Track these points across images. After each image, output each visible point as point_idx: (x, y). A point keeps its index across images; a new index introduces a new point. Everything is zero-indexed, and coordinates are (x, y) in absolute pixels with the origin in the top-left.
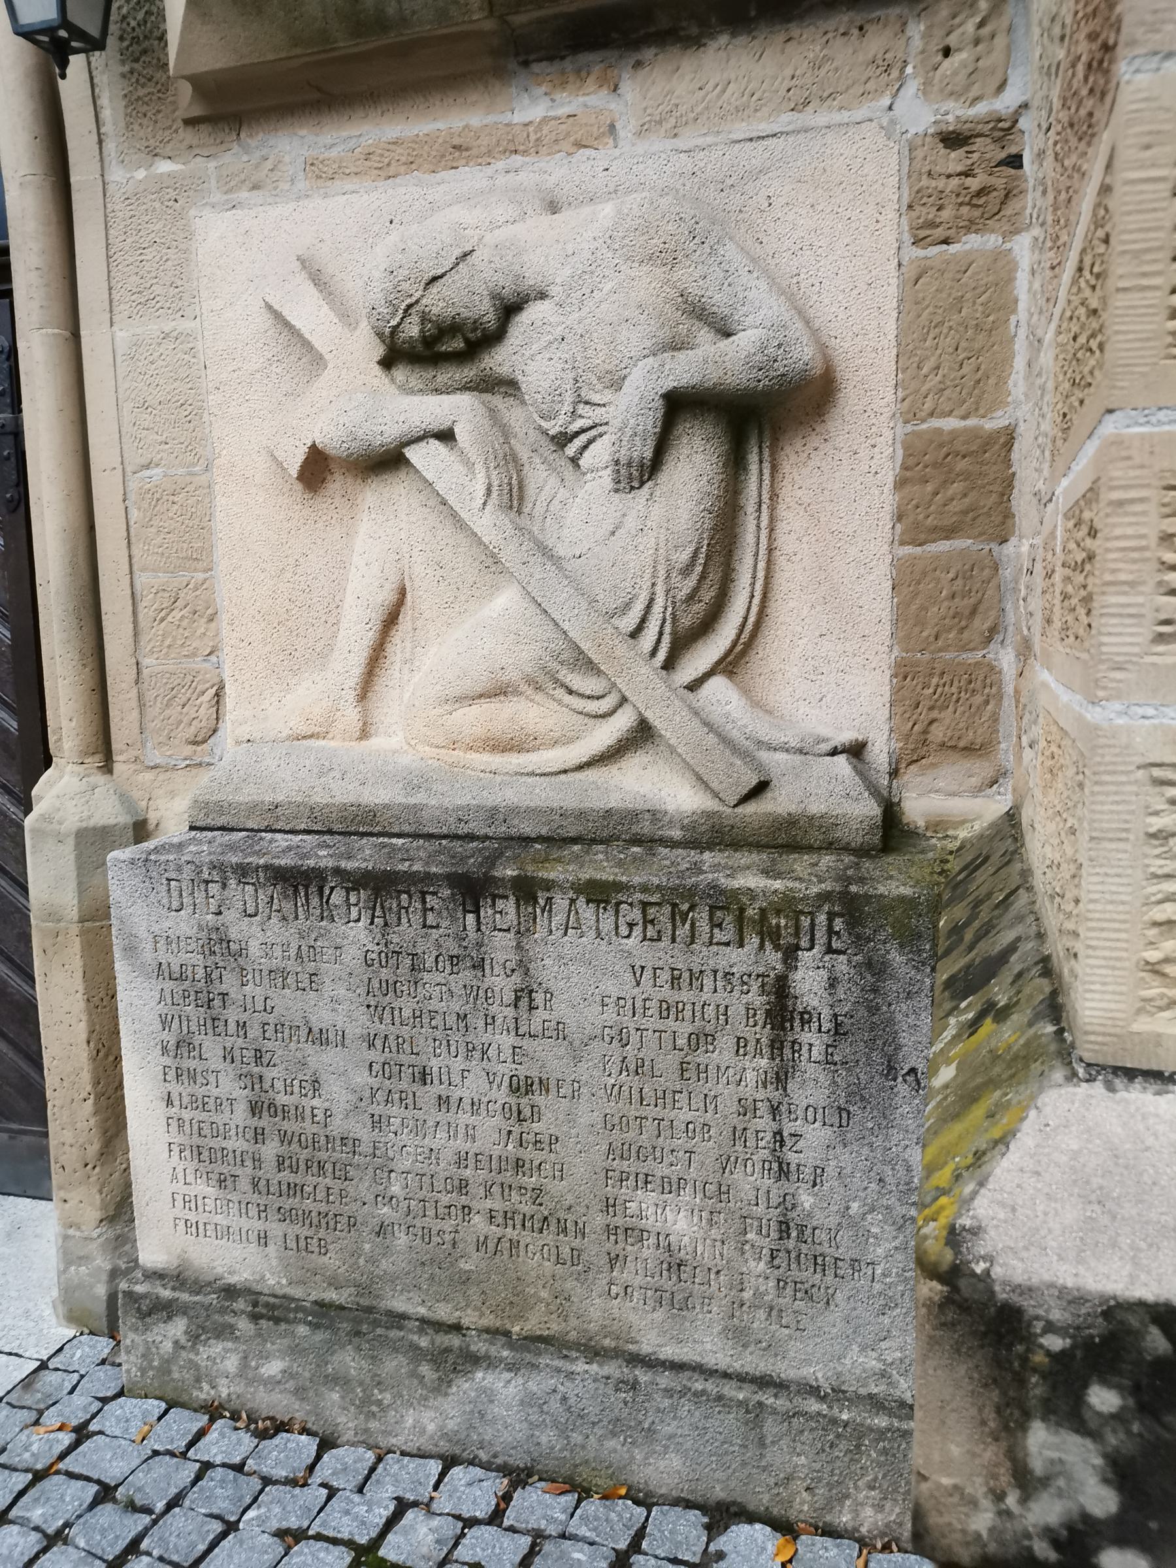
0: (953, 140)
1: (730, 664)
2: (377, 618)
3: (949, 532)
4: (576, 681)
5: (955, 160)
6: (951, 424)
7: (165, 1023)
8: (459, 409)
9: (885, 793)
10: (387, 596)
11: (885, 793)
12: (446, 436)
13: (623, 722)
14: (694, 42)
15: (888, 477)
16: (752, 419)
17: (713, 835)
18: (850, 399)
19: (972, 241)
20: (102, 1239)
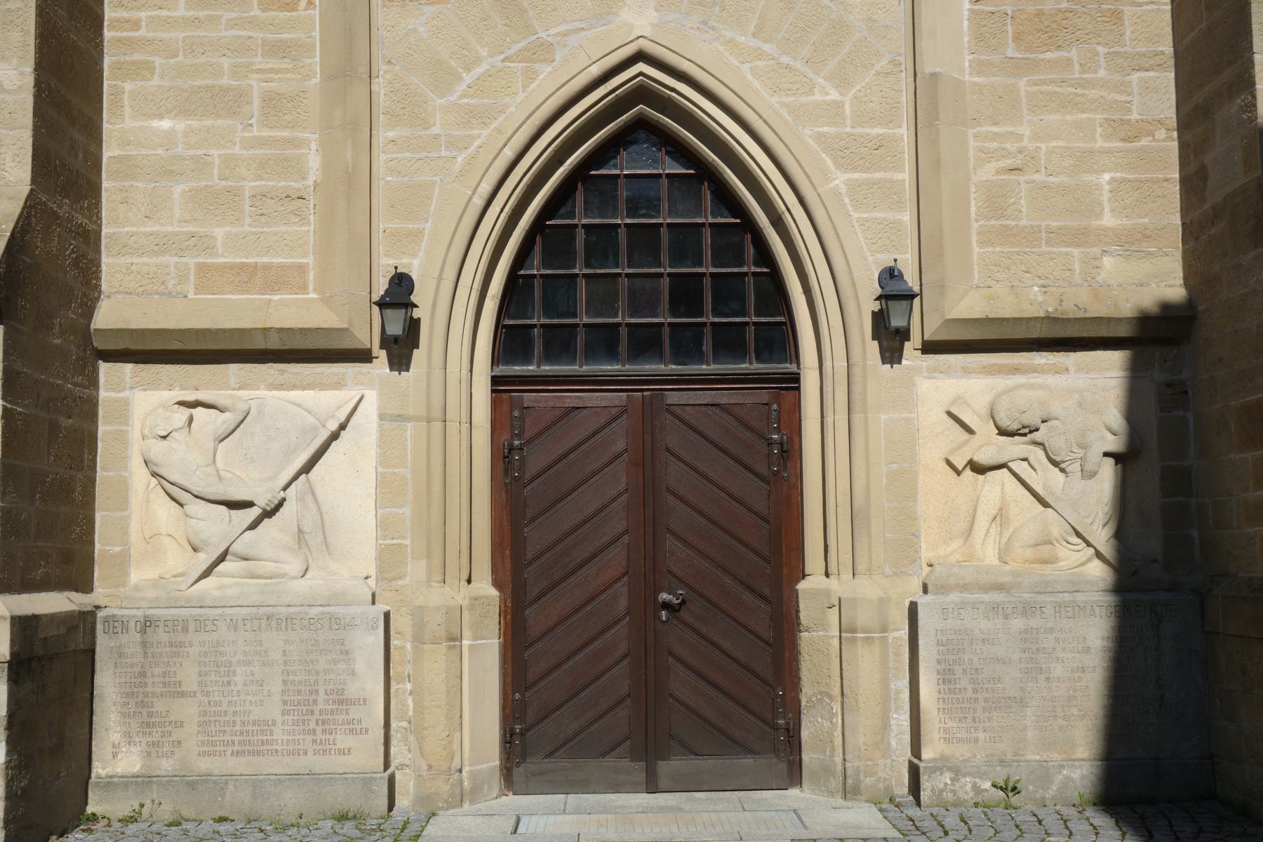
6: (1173, 463)
7: (939, 662)
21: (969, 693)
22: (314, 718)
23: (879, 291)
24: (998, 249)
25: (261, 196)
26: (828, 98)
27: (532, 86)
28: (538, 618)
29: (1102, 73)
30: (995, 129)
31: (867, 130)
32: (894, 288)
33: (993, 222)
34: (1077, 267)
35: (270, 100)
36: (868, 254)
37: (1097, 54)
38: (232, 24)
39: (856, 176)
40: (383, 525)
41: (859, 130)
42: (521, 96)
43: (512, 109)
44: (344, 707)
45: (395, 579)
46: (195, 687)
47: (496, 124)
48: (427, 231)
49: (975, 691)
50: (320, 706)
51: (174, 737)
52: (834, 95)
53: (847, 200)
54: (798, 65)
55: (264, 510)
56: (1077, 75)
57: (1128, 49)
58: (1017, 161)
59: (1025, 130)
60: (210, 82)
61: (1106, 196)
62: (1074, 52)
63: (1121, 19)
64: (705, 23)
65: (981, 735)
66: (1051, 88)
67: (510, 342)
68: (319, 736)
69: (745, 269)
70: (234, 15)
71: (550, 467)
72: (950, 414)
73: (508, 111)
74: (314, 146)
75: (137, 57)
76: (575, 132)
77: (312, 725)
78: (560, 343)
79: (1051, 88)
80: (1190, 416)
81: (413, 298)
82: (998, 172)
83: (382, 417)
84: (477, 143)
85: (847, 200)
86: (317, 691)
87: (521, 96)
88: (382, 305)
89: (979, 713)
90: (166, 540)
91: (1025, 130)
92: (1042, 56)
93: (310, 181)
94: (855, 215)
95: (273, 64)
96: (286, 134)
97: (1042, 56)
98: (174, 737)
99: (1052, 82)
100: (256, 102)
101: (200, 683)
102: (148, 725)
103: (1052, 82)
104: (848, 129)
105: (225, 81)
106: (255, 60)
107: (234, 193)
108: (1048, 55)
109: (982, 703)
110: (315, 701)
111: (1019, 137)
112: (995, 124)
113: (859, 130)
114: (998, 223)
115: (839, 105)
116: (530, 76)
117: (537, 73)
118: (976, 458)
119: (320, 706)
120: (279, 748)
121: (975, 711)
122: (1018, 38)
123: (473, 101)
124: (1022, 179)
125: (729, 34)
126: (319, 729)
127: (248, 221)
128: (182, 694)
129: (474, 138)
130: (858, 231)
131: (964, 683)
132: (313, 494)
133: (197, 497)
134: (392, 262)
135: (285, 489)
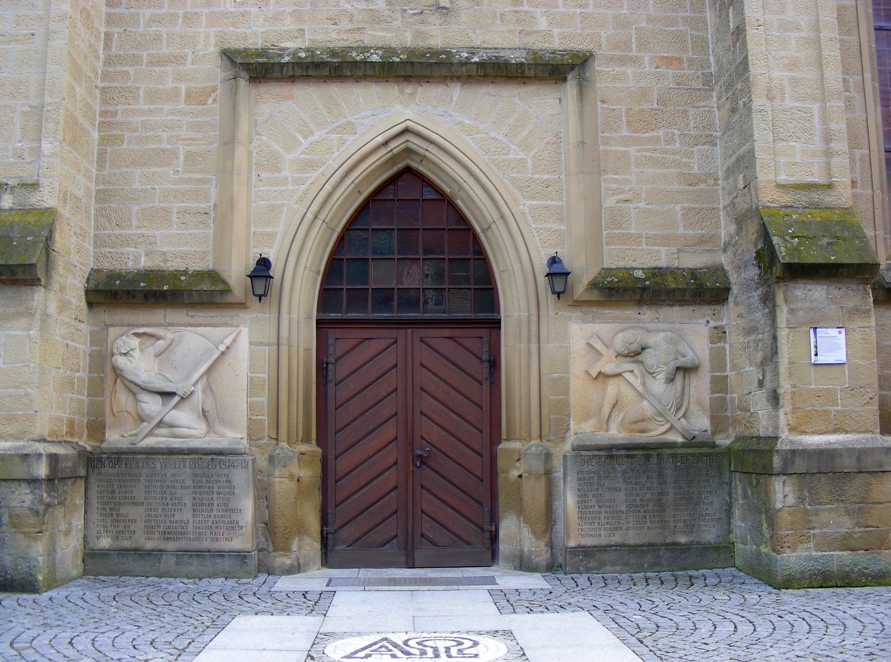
0: (715, 328)
1: (684, 416)
2: (611, 406)
3: (719, 392)
4: (658, 419)
5: (716, 331)
6: (718, 374)
7: (579, 490)
8: (635, 368)
9: (205, 379)
10: (614, 402)
11: (205, 379)
12: (632, 371)
13: (668, 426)
14: (672, 306)
15: (708, 382)
16: (686, 370)
17: (683, 445)
18: (701, 369)
19: (719, 345)
20: (95, 516)
21: (597, 508)
22: (211, 520)
23: (547, 271)
24: (618, 247)
25: (182, 212)
26: (518, 157)
27: (343, 148)
28: (344, 464)
29: (677, 145)
30: (616, 177)
31: (542, 176)
32: (556, 269)
33: (615, 231)
34: (663, 257)
35: (189, 156)
36: (541, 249)
37: (674, 135)
38: (171, 113)
39: (535, 202)
40: (251, 407)
41: (537, 176)
42: (336, 154)
43: (331, 161)
44: (229, 513)
45: (258, 439)
46: (142, 500)
47: (321, 170)
48: (279, 234)
49: (600, 507)
50: (215, 513)
51: (131, 528)
52: (522, 155)
53: (529, 217)
54: (500, 137)
55: (182, 398)
56: (663, 147)
57: (692, 132)
58: (629, 196)
59: (633, 177)
60: (155, 146)
61: (679, 217)
62: (661, 132)
63: (687, 115)
64: (446, 112)
65: (603, 533)
66: (648, 154)
67: (328, 296)
68: (214, 530)
69: (469, 256)
70: (171, 107)
71: (371, 360)
72: (588, 343)
73: (328, 163)
74: (214, 183)
75: (115, 132)
76: (368, 176)
77: (210, 524)
78: (357, 298)
79: (648, 154)
80: (727, 346)
81: (271, 274)
82: (617, 202)
83: (251, 343)
84: (310, 182)
85: (529, 217)
86: (213, 505)
87: (336, 154)
88: (251, 276)
89: (602, 520)
90: (126, 414)
91: (633, 177)
92: (643, 135)
93: (212, 204)
94: (534, 226)
95: (191, 135)
96: (198, 176)
97: (643, 135)
98: (131, 528)
99: (648, 150)
100: (182, 158)
101: (146, 498)
102: (117, 521)
103: (648, 150)
104: (530, 175)
105: (163, 146)
106: (182, 133)
107: (168, 211)
108: (646, 135)
109: (603, 514)
110: (212, 510)
111: (629, 181)
112: (616, 174)
113: (537, 176)
114: (617, 232)
115: (523, 161)
116: (342, 142)
117: (346, 141)
118: (603, 371)
119: (215, 513)
120: (191, 536)
121: (600, 518)
122: (629, 124)
123: (308, 157)
124: (632, 206)
125: (459, 119)
126: (214, 526)
127: (175, 227)
128: (136, 504)
129: (308, 178)
130: (536, 235)
131: (594, 502)
132: (211, 389)
133: (144, 389)
134: (260, 251)
135: (194, 385)
